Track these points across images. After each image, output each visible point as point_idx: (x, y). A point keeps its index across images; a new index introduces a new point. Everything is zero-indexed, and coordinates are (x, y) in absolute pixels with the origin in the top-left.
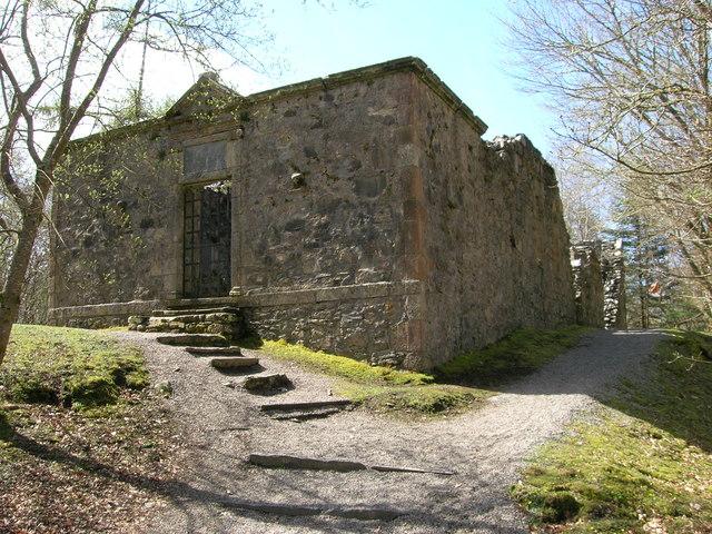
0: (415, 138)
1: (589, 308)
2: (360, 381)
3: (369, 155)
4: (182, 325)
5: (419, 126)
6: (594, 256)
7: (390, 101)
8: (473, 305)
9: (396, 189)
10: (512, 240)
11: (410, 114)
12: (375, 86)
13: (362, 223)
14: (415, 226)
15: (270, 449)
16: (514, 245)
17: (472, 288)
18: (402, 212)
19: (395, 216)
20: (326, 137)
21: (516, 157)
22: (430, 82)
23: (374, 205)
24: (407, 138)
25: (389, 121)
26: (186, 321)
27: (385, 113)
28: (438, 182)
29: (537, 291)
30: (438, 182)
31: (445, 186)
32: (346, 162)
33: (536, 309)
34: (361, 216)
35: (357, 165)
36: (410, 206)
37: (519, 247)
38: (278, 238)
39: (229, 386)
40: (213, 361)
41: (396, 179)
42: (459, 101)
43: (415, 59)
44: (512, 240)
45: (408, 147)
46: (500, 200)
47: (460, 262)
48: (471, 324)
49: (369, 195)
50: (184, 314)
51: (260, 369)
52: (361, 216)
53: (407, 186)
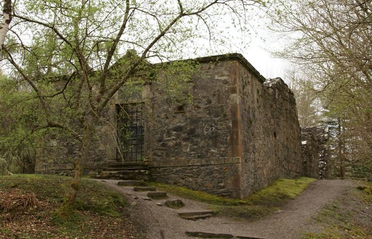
0: (238, 91)
1: (311, 167)
2: (210, 201)
3: (215, 98)
4: (121, 176)
5: (238, 85)
6: (313, 138)
7: (226, 73)
8: (258, 168)
9: (229, 114)
10: (275, 134)
11: (235, 80)
12: (219, 65)
13: (212, 129)
14: (237, 132)
15: (201, 224)
16: (275, 136)
17: (259, 160)
18: (231, 125)
19: (228, 127)
20: (194, 87)
21: (277, 90)
22: (243, 63)
23: (217, 121)
24: (234, 91)
25: (226, 82)
26: (124, 174)
27: (224, 78)
28: (245, 110)
29: (285, 159)
30: (245, 110)
31: (249, 113)
32: (204, 100)
33: (285, 169)
34: (211, 126)
35: (209, 102)
36: (235, 123)
37: (278, 137)
38: (169, 134)
39: (367, 192)
40: (149, 193)
41: (228, 110)
42: (254, 69)
43: (238, 54)
44: (275, 134)
45: (235, 95)
46: (270, 115)
47: (254, 146)
48: (258, 177)
49: (215, 117)
50: (123, 170)
51: (148, 195)
52: (211, 126)
53: (234, 114)
